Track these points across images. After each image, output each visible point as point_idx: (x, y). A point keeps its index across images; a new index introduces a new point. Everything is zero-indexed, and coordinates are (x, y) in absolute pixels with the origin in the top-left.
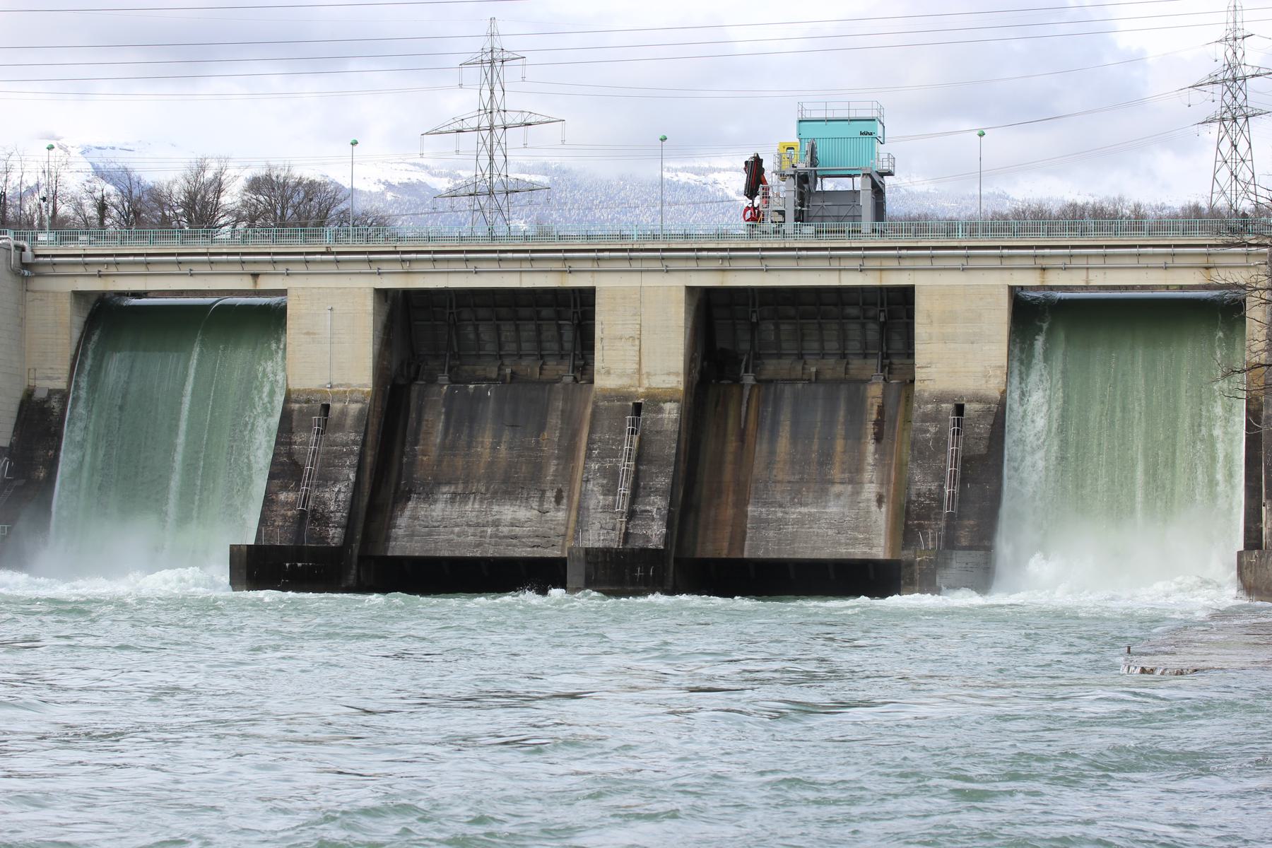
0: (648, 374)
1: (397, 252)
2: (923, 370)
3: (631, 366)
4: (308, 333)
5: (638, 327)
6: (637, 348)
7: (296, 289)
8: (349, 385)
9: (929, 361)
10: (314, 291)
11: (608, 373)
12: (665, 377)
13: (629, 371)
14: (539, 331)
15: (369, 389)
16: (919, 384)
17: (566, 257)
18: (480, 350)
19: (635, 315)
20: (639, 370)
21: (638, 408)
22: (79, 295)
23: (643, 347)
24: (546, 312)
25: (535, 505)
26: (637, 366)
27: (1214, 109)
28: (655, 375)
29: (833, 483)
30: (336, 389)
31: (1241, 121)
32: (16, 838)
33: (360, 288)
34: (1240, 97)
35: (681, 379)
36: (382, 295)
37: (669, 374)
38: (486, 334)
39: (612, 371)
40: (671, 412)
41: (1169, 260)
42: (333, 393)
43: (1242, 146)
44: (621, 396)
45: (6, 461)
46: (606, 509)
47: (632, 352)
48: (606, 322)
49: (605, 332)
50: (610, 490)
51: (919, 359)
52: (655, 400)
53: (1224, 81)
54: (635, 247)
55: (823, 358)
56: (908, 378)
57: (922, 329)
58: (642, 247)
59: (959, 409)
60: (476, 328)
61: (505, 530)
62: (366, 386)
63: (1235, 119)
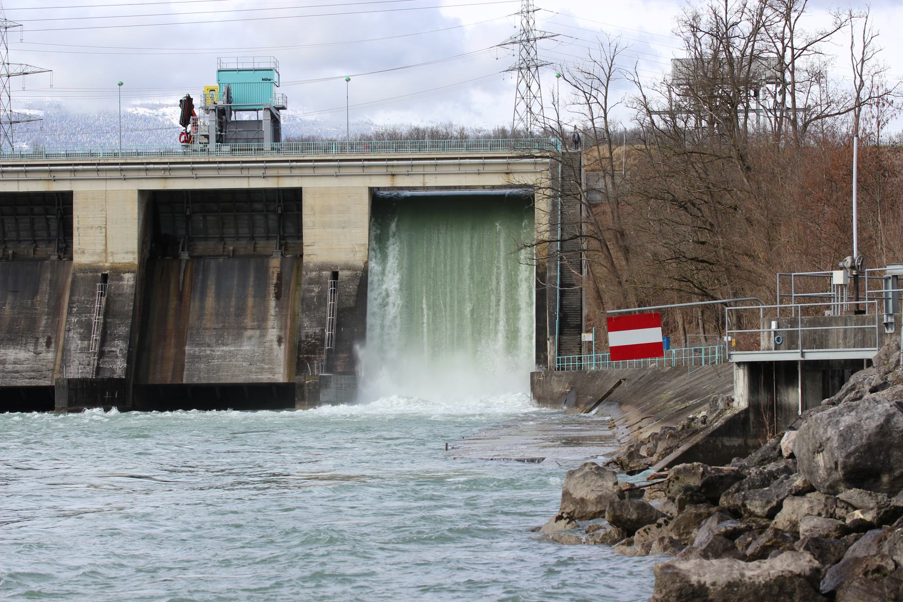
0: (112, 253)
2: (310, 248)
3: (100, 248)
6: (104, 234)
11: (83, 252)
14: (32, 224)
17: (51, 170)
19: (102, 211)
20: (106, 251)
21: (105, 278)
24: (37, 209)
25: (31, 348)
26: (104, 248)
27: (514, 61)
28: (117, 253)
29: (246, 329)
31: (533, 69)
34: (532, 53)
35: (136, 256)
37: (127, 253)
40: (129, 280)
41: (481, 168)
43: (534, 87)
44: (93, 269)
46: (82, 350)
47: (100, 238)
48: (81, 216)
50: (86, 337)
51: (306, 239)
52: (118, 271)
53: (521, 41)
54: (101, 162)
56: (299, 253)
57: (307, 218)
58: (106, 162)
59: (335, 275)
61: (10, 367)
63: (529, 68)
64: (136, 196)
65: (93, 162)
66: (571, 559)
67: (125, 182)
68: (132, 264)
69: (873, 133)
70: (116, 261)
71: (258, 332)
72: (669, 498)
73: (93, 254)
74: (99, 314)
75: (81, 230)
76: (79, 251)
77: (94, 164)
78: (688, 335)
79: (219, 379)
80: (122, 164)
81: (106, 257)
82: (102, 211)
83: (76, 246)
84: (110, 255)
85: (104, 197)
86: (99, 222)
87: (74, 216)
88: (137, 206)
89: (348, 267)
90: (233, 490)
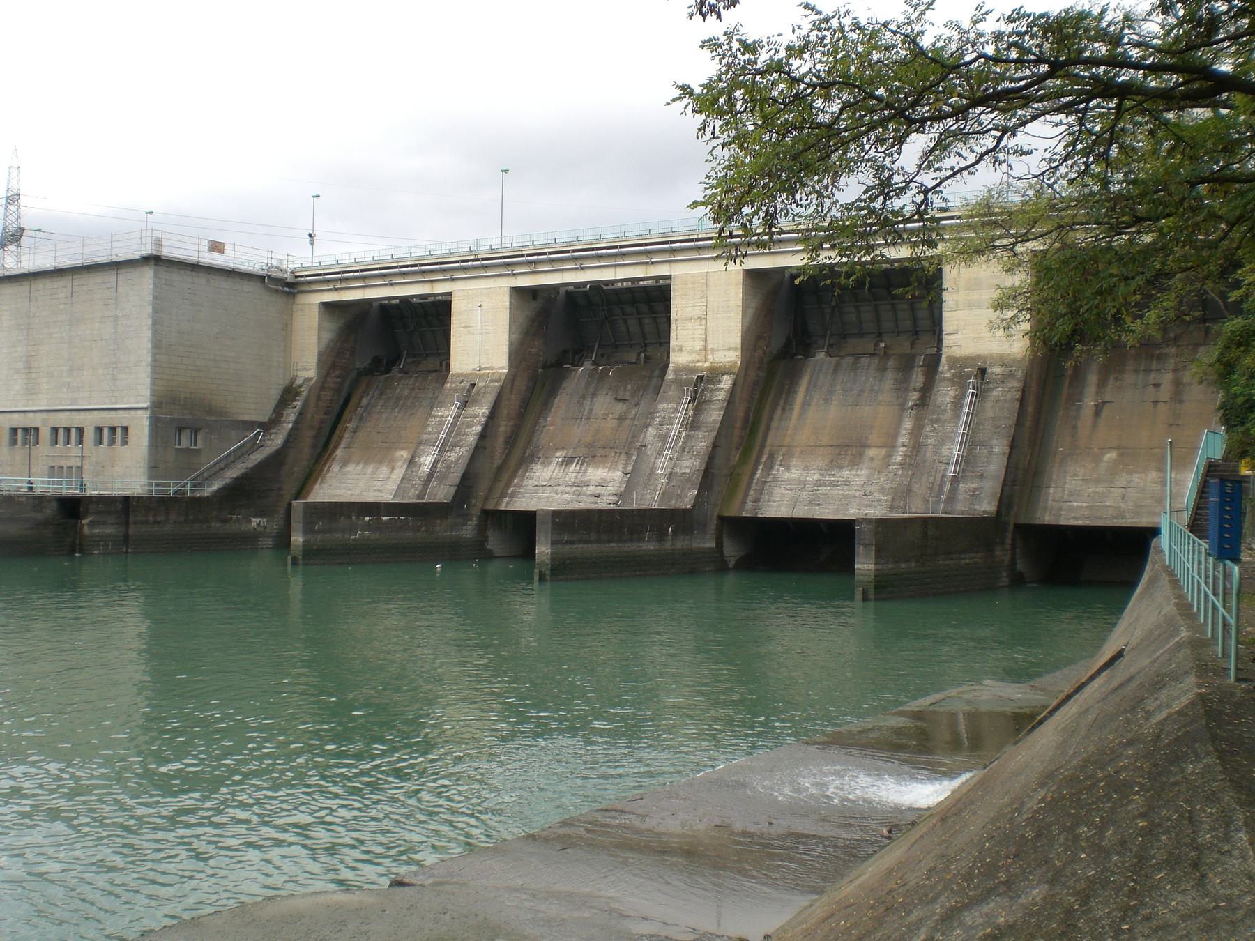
1: (522, 256)
2: (951, 337)
4: (466, 327)
5: (704, 308)
6: (704, 327)
7: (457, 291)
8: (492, 368)
9: (956, 328)
10: (470, 292)
11: (681, 350)
12: (725, 353)
15: (506, 371)
16: (946, 350)
18: (630, 340)
19: (701, 298)
20: (705, 346)
22: (327, 306)
23: (708, 325)
26: (703, 343)
28: (718, 350)
30: (482, 372)
32: (867, 517)
33: (500, 288)
35: (739, 353)
36: (520, 294)
37: (729, 349)
38: (633, 324)
39: (684, 349)
40: (726, 383)
42: (481, 376)
44: (690, 370)
45: (260, 432)
47: (700, 332)
48: (681, 306)
49: (679, 314)
51: (947, 326)
52: (714, 375)
54: (700, 236)
55: (898, 335)
58: (705, 236)
59: (982, 372)
60: (625, 321)
62: (503, 368)
66: (303, 898)
73: (693, 351)
77: (691, 240)
79: (471, 445)
83: (673, 343)
86: (698, 312)
89: (1002, 360)
90: (123, 605)
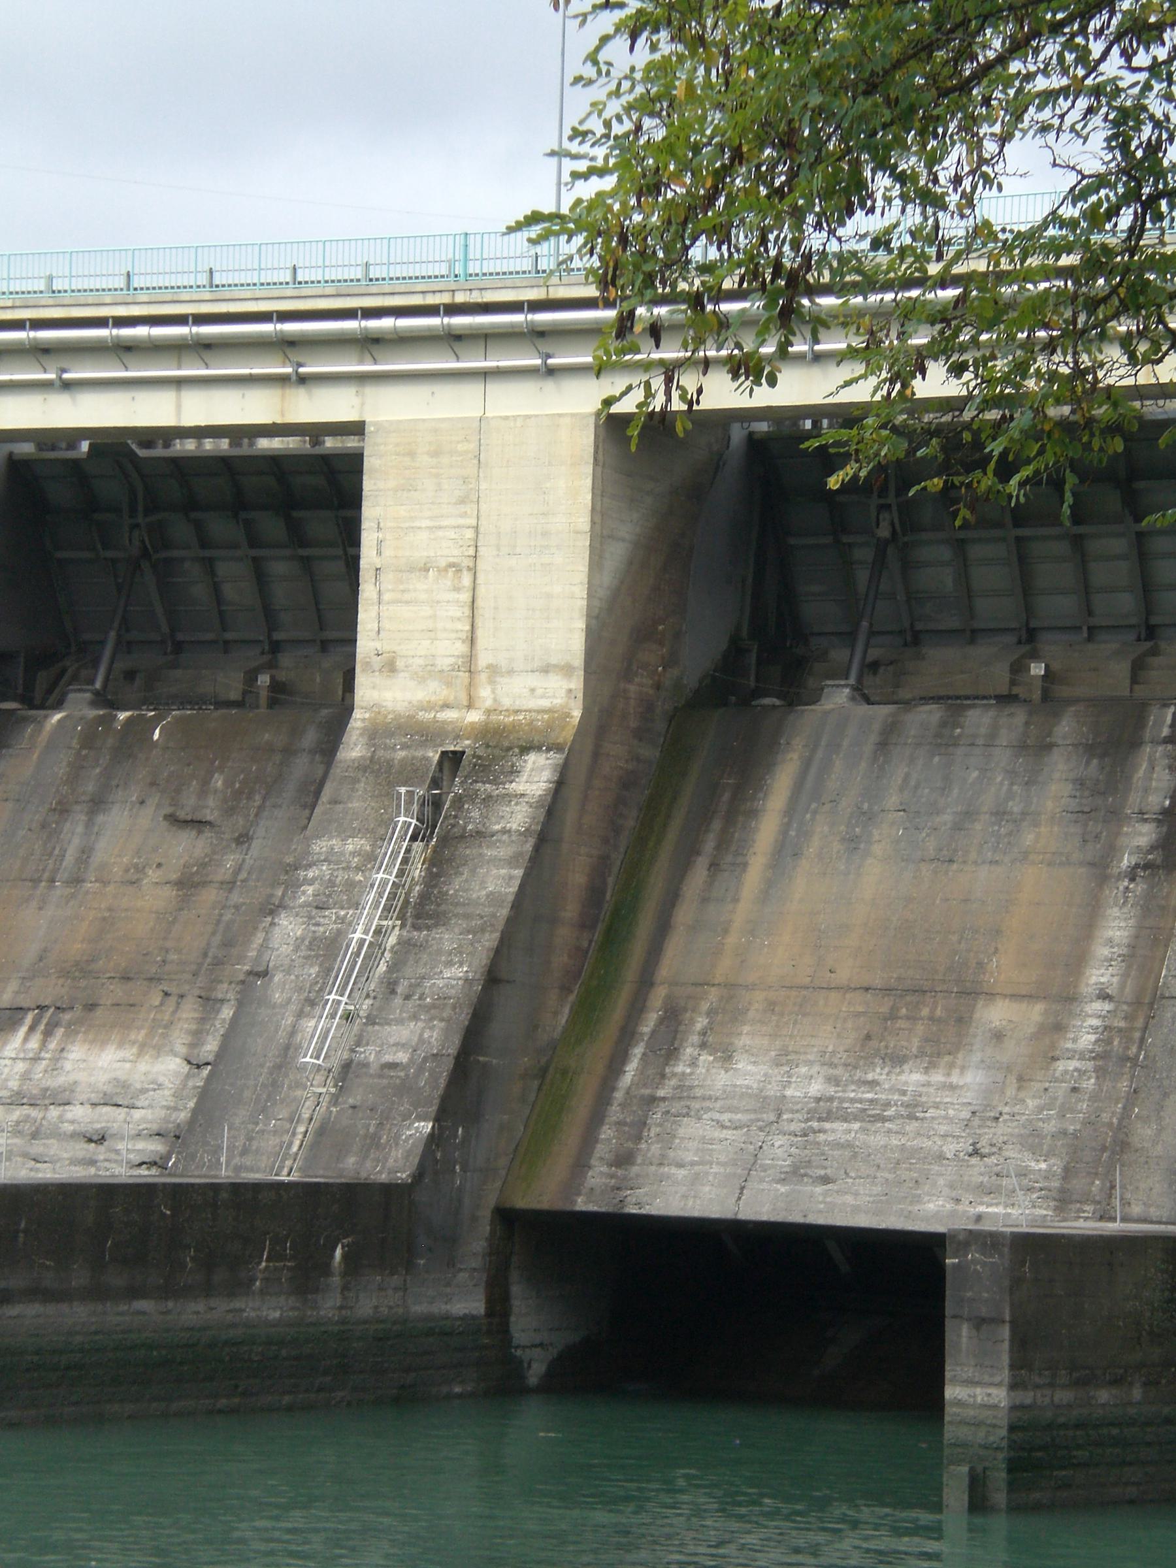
0: (494, 670)
3: (450, 649)
6: (465, 597)
11: (390, 667)
12: (535, 680)
13: (445, 663)
19: (462, 501)
20: (469, 663)
28: (511, 672)
35: (577, 683)
37: (546, 670)
47: (453, 611)
54: (460, 298)
58: (476, 298)
64: (585, 440)
65: (431, 300)
67: (549, 385)
68: (558, 716)
69: (1106, 119)
70: (507, 703)
71: (1036, 1012)
72: (1062, 1190)
73: (428, 672)
74: (387, 909)
75: (387, 579)
76: (377, 662)
78: (869, 651)
80: (537, 306)
81: (471, 686)
82: (462, 501)
83: (366, 644)
84: (483, 677)
85: (472, 446)
86: (449, 548)
87: (365, 525)
88: (588, 482)
